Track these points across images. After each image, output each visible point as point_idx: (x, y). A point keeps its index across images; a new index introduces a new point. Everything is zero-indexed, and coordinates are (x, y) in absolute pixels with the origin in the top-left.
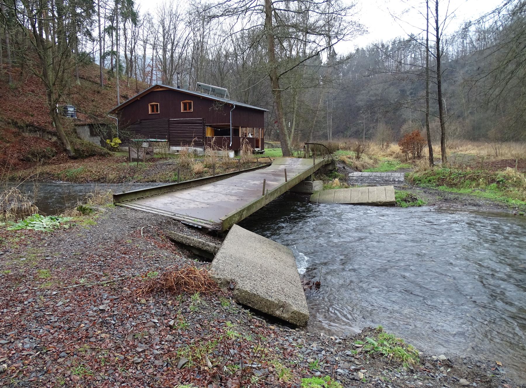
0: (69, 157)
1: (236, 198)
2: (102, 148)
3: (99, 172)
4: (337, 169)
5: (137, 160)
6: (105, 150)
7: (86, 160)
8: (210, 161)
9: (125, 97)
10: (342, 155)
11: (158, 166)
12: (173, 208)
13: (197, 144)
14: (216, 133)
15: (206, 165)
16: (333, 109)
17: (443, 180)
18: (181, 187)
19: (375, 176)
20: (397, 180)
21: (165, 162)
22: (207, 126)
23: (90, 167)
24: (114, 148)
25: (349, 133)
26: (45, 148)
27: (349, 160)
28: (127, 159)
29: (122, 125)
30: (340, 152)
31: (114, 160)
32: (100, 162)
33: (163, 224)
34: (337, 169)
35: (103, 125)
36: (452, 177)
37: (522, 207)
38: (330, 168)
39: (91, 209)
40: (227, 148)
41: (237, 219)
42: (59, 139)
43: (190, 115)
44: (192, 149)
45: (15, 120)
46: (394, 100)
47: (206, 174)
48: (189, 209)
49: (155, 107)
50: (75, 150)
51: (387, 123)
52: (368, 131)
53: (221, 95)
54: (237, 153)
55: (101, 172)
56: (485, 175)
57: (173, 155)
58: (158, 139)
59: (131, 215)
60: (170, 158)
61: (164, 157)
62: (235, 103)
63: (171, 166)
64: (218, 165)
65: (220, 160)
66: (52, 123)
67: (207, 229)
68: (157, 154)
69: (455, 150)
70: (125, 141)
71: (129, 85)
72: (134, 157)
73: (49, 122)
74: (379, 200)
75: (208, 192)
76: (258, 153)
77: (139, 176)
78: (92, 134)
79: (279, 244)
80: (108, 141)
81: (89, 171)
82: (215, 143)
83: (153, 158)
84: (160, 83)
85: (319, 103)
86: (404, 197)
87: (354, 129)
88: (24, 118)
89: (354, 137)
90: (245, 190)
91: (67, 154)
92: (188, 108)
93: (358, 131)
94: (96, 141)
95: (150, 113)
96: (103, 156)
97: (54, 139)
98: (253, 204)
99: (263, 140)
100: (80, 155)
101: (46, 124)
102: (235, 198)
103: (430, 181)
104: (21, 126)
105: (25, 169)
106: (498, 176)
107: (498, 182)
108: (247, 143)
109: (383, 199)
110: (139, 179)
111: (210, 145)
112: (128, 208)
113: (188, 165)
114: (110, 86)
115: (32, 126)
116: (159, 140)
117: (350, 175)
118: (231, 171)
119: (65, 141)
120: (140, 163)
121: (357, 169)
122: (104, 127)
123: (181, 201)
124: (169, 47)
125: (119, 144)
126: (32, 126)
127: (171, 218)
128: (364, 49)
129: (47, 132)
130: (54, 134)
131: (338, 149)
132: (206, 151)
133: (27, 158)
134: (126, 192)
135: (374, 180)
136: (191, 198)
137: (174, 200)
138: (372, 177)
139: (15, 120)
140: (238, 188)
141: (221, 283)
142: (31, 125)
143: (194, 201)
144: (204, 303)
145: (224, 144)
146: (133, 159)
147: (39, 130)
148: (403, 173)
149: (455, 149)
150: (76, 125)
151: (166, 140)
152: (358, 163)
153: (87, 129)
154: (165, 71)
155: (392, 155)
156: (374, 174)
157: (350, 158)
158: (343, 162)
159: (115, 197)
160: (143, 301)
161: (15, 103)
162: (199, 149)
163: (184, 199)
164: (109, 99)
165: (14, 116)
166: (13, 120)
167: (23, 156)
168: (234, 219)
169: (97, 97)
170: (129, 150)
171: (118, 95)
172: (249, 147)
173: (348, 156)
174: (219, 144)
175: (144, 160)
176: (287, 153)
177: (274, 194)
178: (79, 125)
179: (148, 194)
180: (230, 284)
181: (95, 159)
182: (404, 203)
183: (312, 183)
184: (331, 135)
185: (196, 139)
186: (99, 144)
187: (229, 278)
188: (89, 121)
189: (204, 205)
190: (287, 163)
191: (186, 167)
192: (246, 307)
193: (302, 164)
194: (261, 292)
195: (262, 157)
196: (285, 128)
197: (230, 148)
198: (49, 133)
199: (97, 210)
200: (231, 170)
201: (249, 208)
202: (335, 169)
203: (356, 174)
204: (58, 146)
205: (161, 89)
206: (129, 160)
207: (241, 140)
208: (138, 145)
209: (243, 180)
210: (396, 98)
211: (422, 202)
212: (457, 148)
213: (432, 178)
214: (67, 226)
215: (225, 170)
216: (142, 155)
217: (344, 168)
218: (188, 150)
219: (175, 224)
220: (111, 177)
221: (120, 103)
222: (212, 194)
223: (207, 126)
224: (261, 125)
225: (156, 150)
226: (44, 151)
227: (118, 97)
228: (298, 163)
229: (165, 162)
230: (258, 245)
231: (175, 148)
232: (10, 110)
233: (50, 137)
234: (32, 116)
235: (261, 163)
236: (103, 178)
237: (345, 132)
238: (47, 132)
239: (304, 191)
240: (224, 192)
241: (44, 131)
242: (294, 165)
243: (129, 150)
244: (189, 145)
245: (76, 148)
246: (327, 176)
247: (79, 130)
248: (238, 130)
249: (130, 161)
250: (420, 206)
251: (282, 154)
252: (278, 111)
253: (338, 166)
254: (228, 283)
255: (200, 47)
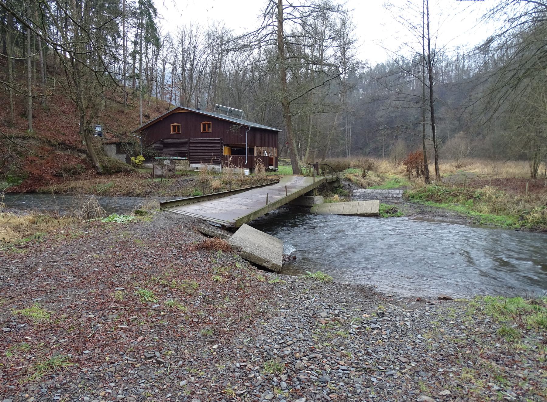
0: (97, 173)
1: (247, 207)
2: (128, 165)
3: (127, 187)
4: (342, 186)
5: (161, 176)
6: (131, 167)
7: (113, 176)
8: (227, 178)
9: (147, 117)
10: (351, 173)
11: (181, 182)
12: (202, 213)
13: (216, 162)
14: (233, 152)
15: (224, 182)
16: (352, 125)
17: (432, 196)
18: (206, 199)
19: (377, 193)
20: (395, 196)
21: (186, 178)
22: (224, 145)
23: (119, 182)
24: (138, 165)
25: (368, 150)
26: (76, 165)
27: (355, 178)
28: (151, 175)
29: (147, 145)
30: (351, 170)
31: (138, 176)
32: (126, 178)
33: (196, 222)
34: (342, 186)
35: (129, 144)
36: (440, 193)
37: (477, 217)
38: (336, 185)
39: (146, 212)
40: (243, 166)
41: (246, 220)
42: (88, 156)
43: (209, 135)
44: (210, 166)
45: (49, 139)
46: (414, 117)
47: (223, 190)
48: (212, 213)
49: (176, 127)
50: (103, 166)
51: (406, 139)
52: (387, 147)
53: (238, 115)
54: (251, 170)
55: (129, 187)
56: (466, 192)
57: (192, 172)
58: (179, 157)
59: (173, 216)
60: (190, 175)
61: (185, 174)
62: (250, 124)
63: (192, 182)
64: (234, 182)
65: (236, 177)
66: (82, 142)
67: (225, 226)
68: (178, 171)
69: (465, 169)
70: (148, 159)
71: (150, 105)
72: (158, 174)
73: (79, 141)
74: (365, 212)
75: (226, 203)
76: (272, 170)
77: (164, 191)
78: (119, 152)
79: (276, 238)
80: (133, 159)
81: (118, 186)
82: (231, 162)
83: (174, 175)
84: (179, 105)
85: (334, 121)
86: (386, 209)
87: (372, 146)
88: (56, 137)
89: (373, 154)
90: (254, 202)
91: (96, 170)
92: (207, 129)
93: (378, 148)
94: (122, 159)
95: (172, 133)
96: (128, 172)
97: (84, 156)
98: (258, 211)
99: (276, 158)
100: (108, 171)
101: (76, 143)
102: (245, 207)
103: (421, 197)
104: (54, 145)
105: (58, 184)
106: (476, 193)
107: (475, 198)
108: (260, 162)
109: (369, 211)
110: (163, 193)
111: (227, 164)
112: (170, 212)
113: (207, 181)
114: (132, 105)
115: (64, 144)
116: (180, 158)
117: (354, 191)
118: (246, 187)
119: (95, 159)
120: (163, 179)
121: (362, 186)
122: (132, 146)
123: (206, 208)
124: (188, 65)
125: (143, 161)
126: (64, 144)
127: (200, 219)
128: (384, 64)
129: (78, 150)
130: (84, 152)
131: (349, 168)
132: (224, 168)
133: (60, 173)
134: (169, 201)
135: (375, 196)
136: (213, 206)
137: (201, 208)
138: (373, 194)
139: (49, 139)
140: (248, 200)
141: (234, 248)
142: (63, 143)
143: (216, 209)
144: (224, 255)
145: (240, 163)
146: (156, 175)
147: (70, 148)
148: (402, 191)
149: (465, 167)
150: (103, 144)
151: (186, 158)
152: (363, 181)
153: (114, 148)
154: (184, 89)
155: (402, 173)
156: (376, 191)
157: (356, 176)
158: (349, 180)
159: (161, 204)
160: (193, 252)
161: (48, 123)
162: (217, 167)
163: (208, 207)
164: (132, 118)
165: (49, 135)
166: (47, 139)
167: (56, 172)
168: (244, 220)
169: (121, 117)
170: (153, 167)
171: (141, 115)
172: (262, 166)
173: (356, 174)
174: (236, 163)
175: (167, 176)
176: (297, 171)
177: (276, 205)
178: (107, 144)
179: (182, 203)
180: (238, 249)
181: (121, 175)
182: (385, 215)
183: (313, 198)
184: (350, 152)
185: (215, 158)
186: (124, 161)
187: (238, 246)
188: (116, 140)
189: (222, 211)
190: (293, 181)
191: (205, 183)
192: (246, 260)
193: (305, 182)
194: (256, 253)
195: (275, 175)
196: (296, 149)
197: (245, 166)
198: (79, 151)
199: (150, 213)
200: (246, 186)
201: (255, 213)
202: (340, 186)
203: (360, 191)
204: (87, 163)
205: (182, 111)
206: (152, 176)
207: (255, 160)
208: (161, 162)
209: (254, 194)
210: (416, 115)
211: (400, 213)
212: (467, 167)
213: (422, 194)
214: (136, 221)
215: (240, 187)
216: (165, 172)
217: (349, 185)
218: (206, 167)
219: (203, 223)
220: (138, 191)
221: (143, 123)
222: (229, 204)
223: (224, 145)
224: (275, 145)
225: (178, 168)
226: (75, 168)
227: (141, 117)
228: (303, 180)
229: (186, 178)
230: (259, 236)
231: (194, 166)
232: (44, 130)
233: (80, 154)
234: (63, 135)
235: (272, 180)
236: (131, 192)
237: (365, 149)
238: (78, 150)
239: (308, 205)
240: (238, 203)
241: (74, 149)
242: (299, 182)
243: (153, 167)
244: (209, 163)
245: (104, 165)
246: (332, 192)
247: (107, 148)
248: (253, 149)
249: (154, 177)
250: (399, 217)
251: (292, 172)
252: (289, 133)
253: (343, 183)
254: (237, 248)
255: (217, 64)
